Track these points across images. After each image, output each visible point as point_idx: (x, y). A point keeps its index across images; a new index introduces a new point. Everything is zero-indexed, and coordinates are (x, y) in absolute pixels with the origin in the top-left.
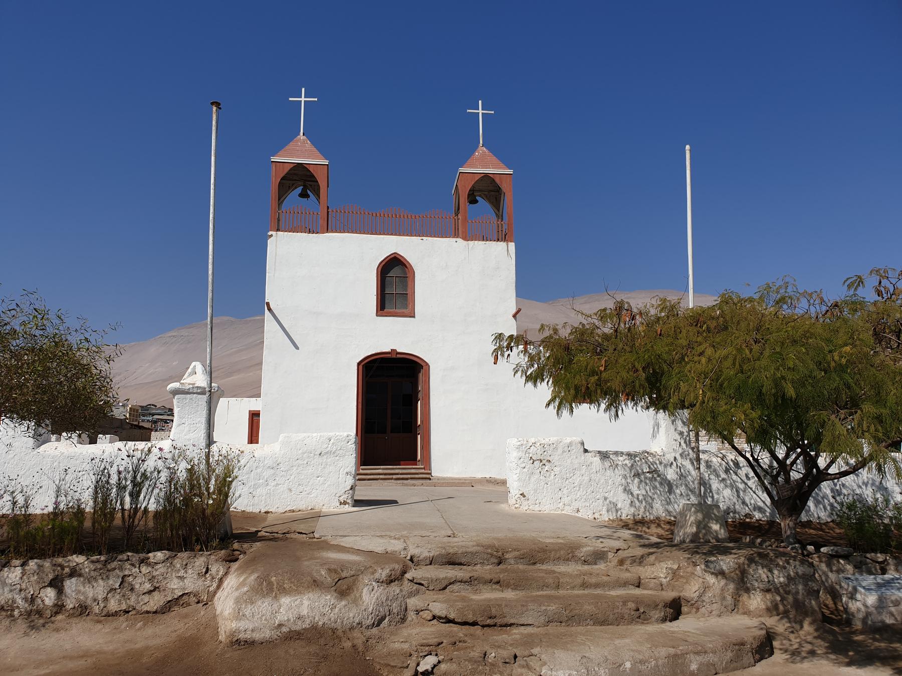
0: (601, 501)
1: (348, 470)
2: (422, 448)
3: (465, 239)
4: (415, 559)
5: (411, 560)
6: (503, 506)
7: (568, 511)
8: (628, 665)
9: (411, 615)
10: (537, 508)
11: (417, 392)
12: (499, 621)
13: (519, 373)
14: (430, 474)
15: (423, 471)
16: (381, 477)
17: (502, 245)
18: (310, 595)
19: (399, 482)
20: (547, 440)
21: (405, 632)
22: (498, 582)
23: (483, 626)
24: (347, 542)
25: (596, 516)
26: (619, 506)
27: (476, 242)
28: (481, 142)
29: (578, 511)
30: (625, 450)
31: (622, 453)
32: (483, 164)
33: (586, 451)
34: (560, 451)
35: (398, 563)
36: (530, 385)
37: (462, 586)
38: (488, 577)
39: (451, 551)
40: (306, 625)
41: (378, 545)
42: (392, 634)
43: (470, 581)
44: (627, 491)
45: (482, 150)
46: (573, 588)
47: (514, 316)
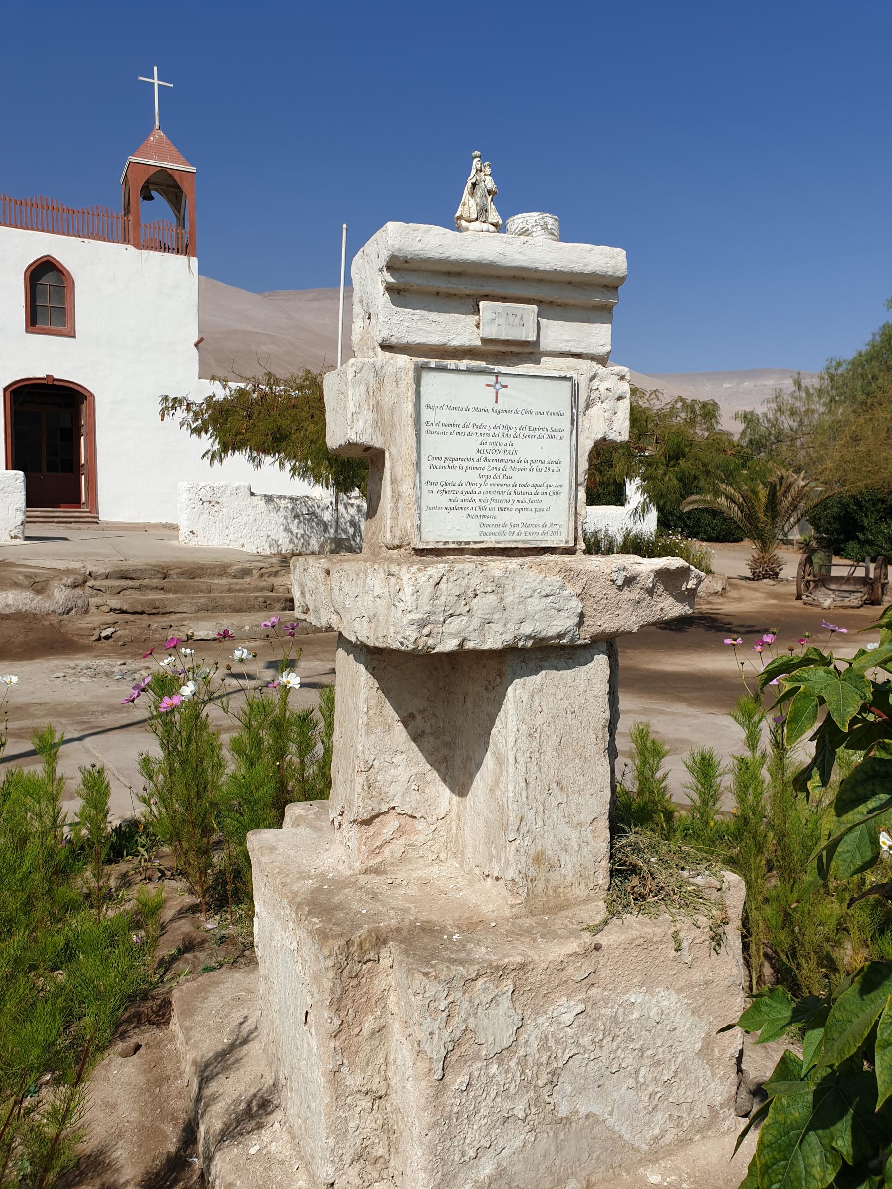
0: (264, 538)
1: (18, 506)
2: (87, 489)
3: (138, 246)
4: (93, 575)
5: (90, 574)
6: (175, 543)
7: (234, 546)
8: (247, 627)
9: (93, 609)
10: (205, 544)
11: (79, 426)
12: (161, 610)
13: (185, 426)
14: (97, 517)
15: (89, 514)
16: (40, 519)
17: (183, 258)
18: (14, 591)
19: (61, 525)
20: (217, 484)
21: (88, 619)
22: (162, 589)
23: (149, 614)
24: (28, 563)
25: (260, 550)
26: (280, 542)
27: (151, 252)
28: (157, 123)
29: (243, 546)
30: (288, 495)
31: (285, 497)
32: (157, 155)
33: (252, 494)
34: (228, 494)
35: (80, 574)
36: (195, 436)
37: (133, 591)
38: (155, 585)
39: (124, 568)
40: (13, 611)
41: (61, 565)
42: (79, 619)
43: (139, 588)
44: (287, 529)
45: (157, 135)
46: (221, 592)
47: (196, 345)
